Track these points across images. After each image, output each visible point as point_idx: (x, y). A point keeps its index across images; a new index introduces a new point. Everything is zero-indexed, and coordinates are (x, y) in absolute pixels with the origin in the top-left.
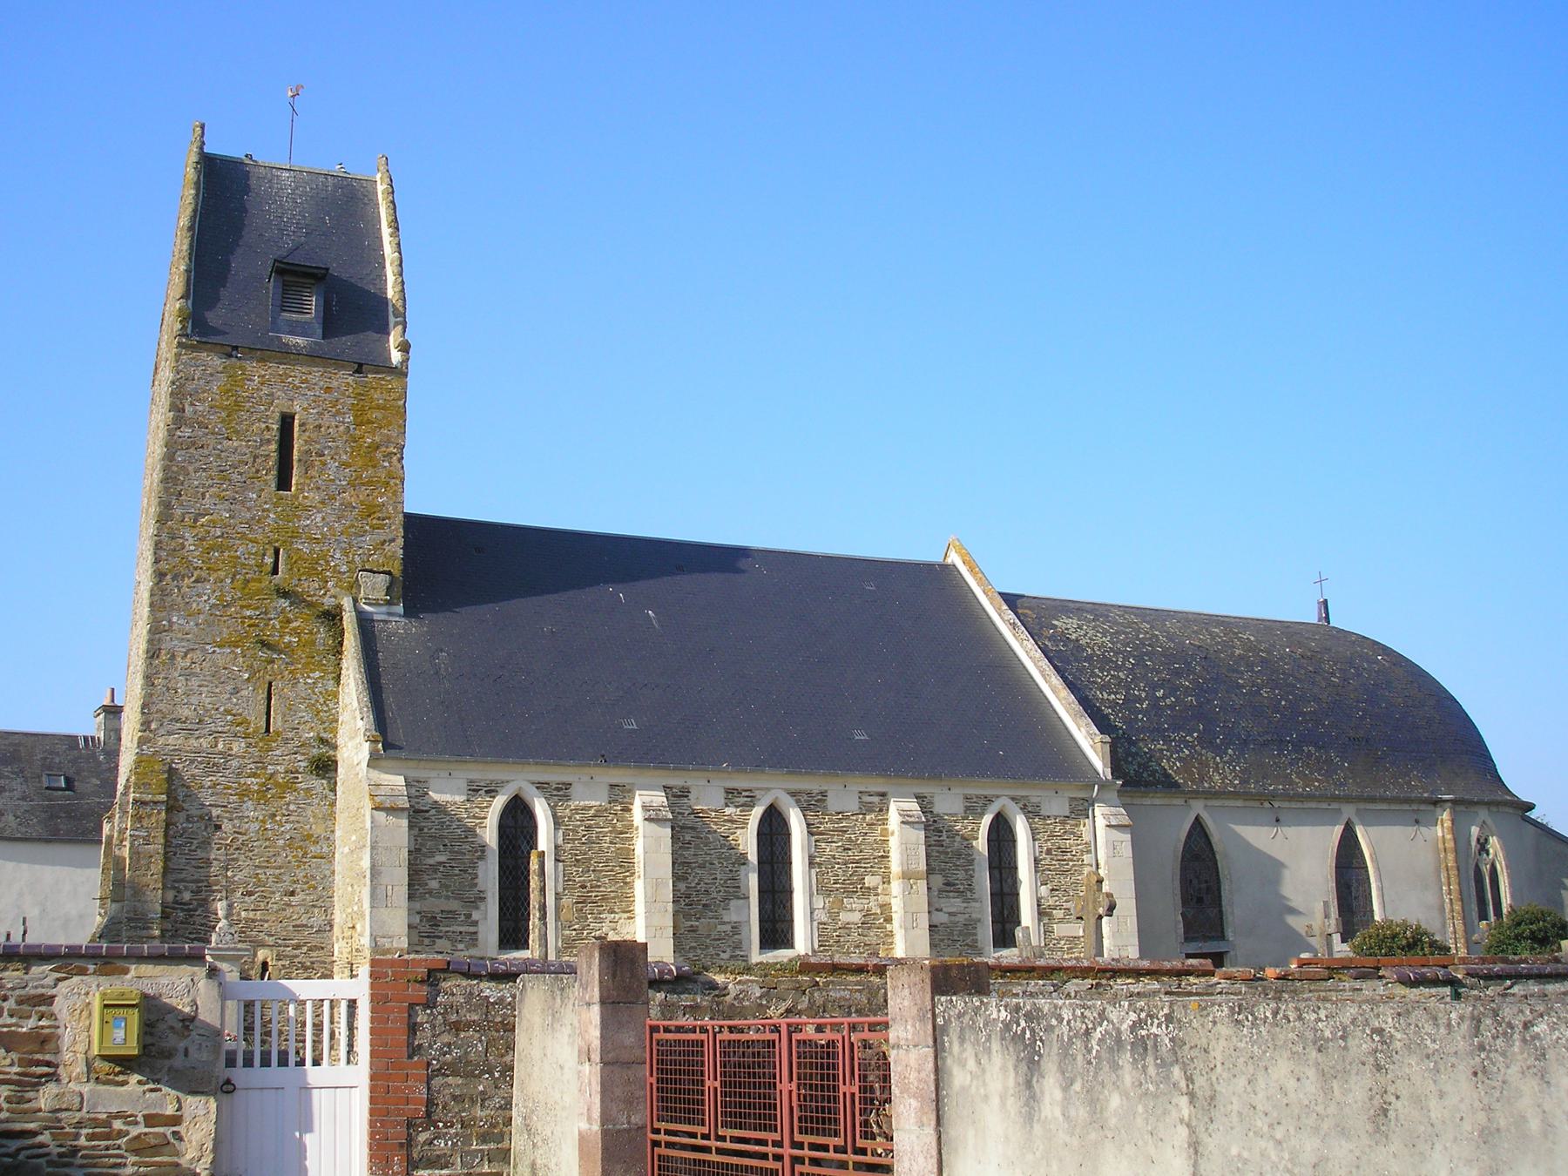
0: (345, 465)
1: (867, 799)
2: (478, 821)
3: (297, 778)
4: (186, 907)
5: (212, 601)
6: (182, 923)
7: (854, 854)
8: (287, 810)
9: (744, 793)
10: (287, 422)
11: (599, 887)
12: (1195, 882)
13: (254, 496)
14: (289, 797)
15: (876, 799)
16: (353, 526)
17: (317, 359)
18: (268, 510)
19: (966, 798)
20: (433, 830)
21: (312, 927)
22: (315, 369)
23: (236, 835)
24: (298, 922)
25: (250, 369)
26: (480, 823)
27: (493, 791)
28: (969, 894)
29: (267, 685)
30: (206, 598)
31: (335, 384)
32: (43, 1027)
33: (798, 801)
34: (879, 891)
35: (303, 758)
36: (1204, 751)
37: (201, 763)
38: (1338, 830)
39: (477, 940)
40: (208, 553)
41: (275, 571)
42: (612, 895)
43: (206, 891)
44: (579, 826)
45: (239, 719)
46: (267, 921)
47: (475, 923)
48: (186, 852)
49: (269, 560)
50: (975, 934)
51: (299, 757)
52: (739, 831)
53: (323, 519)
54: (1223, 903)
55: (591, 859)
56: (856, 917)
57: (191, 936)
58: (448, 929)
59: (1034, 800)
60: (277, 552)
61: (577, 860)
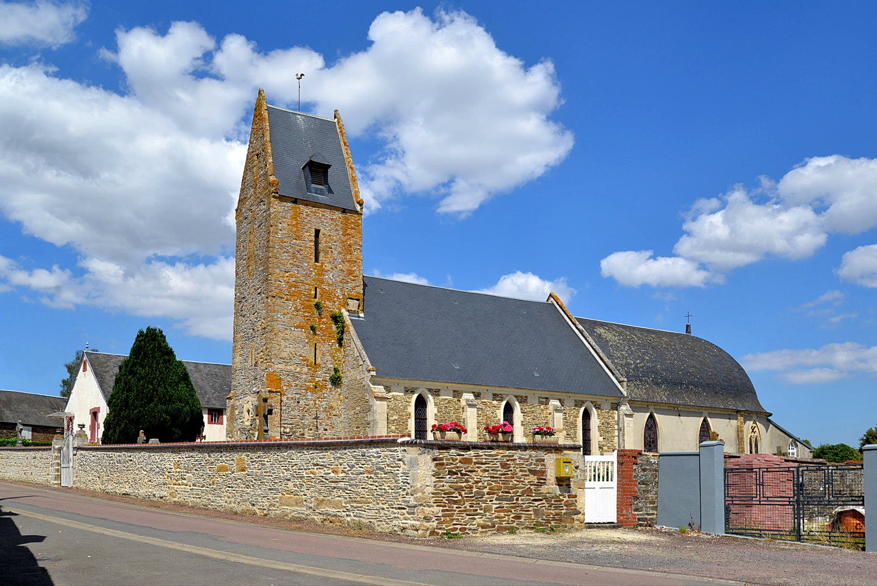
0: (340, 253)
1: (541, 400)
2: (408, 403)
4: (287, 434)
5: (293, 309)
8: (323, 396)
9: (499, 396)
10: (317, 232)
12: (648, 438)
13: (306, 265)
14: (324, 391)
15: (544, 400)
16: (344, 280)
18: (311, 271)
22: (327, 210)
27: (413, 392)
28: (575, 439)
29: (314, 345)
30: (290, 307)
31: (334, 217)
32: (542, 468)
33: (518, 400)
36: (654, 386)
37: (291, 376)
38: (702, 419)
41: (315, 297)
45: (305, 358)
48: (287, 412)
49: (313, 292)
51: (328, 375)
52: (497, 411)
53: (333, 276)
54: (658, 448)
55: (447, 420)
60: (316, 288)
61: (442, 420)
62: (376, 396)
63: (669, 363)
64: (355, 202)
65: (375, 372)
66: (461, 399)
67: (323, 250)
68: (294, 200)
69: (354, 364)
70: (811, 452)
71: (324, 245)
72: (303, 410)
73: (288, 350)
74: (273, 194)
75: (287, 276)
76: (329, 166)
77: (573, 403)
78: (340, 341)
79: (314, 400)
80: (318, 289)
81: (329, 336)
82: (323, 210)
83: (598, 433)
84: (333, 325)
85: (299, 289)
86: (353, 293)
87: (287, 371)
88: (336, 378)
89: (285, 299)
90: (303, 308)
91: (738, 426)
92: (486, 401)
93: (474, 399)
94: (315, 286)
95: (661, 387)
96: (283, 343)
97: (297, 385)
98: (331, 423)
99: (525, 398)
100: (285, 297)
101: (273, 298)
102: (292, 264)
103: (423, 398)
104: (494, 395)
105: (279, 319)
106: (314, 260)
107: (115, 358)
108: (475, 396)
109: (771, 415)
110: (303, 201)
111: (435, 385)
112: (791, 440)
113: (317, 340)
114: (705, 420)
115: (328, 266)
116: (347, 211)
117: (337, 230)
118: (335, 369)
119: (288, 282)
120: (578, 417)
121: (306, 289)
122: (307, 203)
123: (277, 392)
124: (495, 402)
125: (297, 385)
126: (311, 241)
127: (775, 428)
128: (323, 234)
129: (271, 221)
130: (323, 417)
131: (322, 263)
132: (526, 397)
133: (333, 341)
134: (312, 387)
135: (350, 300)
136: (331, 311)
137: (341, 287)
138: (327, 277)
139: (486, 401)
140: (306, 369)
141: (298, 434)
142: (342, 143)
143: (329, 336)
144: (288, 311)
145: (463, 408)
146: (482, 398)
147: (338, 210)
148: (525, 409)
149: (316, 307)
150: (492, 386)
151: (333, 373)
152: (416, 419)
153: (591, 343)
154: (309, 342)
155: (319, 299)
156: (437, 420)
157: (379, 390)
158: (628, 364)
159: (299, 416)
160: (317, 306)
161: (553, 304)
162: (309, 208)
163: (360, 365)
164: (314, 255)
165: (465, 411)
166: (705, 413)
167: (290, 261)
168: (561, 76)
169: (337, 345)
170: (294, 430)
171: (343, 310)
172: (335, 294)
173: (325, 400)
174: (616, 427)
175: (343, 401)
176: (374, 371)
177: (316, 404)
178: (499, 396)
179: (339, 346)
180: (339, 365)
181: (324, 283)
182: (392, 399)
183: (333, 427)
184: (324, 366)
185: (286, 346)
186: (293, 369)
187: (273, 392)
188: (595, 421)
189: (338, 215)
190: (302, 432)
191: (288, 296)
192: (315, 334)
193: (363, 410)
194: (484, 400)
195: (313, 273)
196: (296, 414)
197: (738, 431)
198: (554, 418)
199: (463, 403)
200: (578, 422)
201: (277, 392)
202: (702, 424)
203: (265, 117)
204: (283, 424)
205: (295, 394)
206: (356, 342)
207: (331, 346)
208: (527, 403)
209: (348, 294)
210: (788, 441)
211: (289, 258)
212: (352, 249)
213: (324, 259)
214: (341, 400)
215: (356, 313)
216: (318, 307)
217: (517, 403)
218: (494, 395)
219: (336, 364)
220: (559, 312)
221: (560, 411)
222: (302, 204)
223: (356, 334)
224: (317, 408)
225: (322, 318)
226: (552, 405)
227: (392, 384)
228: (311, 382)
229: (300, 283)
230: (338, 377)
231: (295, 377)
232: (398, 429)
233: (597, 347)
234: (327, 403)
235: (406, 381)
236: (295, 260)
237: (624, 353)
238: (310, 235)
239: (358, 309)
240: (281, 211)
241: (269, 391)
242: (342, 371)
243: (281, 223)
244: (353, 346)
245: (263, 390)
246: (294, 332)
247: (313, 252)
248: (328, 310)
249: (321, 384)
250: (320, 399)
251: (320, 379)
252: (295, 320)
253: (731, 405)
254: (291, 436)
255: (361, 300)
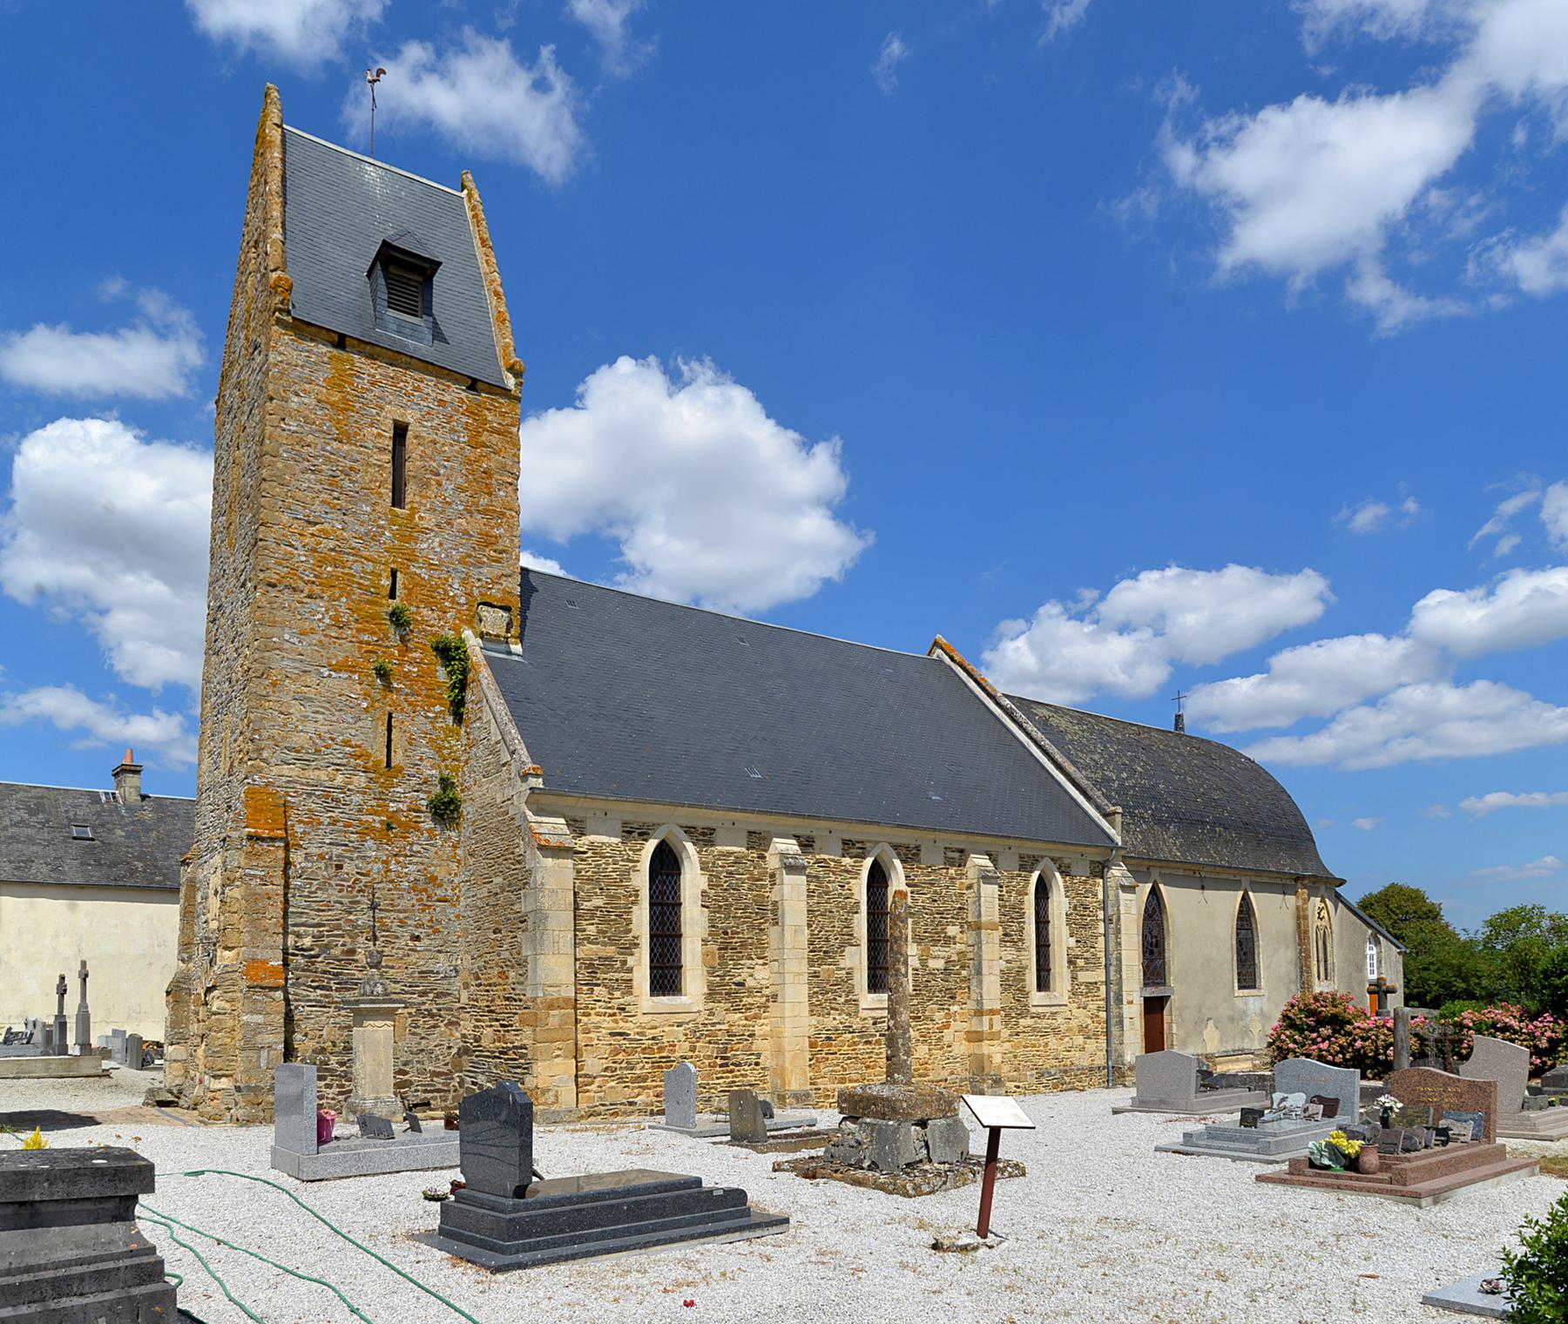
0: (462, 489)
1: (950, 855)
2: (631, 864)
3: (420, 817)
5: (327, 621)
6: (303, 970)
7: (940, 905)
8: (411, 850)
9: (857, 845)
10: (400, 431)
11: (738, 933)
13: (368, 509)
14: (412, 838)
15: (956, 855)
16: (470, 556)
17: (430, 367)
18: (382, 527)
19: (1021, 857)
20: (590, 873)
21: (438, 973)
23: (359, 876)
24: (424, 969)
25: (358, 364)
26: (634, 866)
28: (1020, 944)
29: (387, 717)
30: (320, 616)
31: (447, 398)
33: (899, 855)
34: (957, 940)
35: (424, 796)
36: (1156, 827)
39: (631, 987)
40: (321, 567)
41: (392, 595)
42: (750, 941)
43: (328, 936)
44: (722, 872)
46: (393, 967)
47: (630, 970)
48: (306, 894)
49: (386, 582)
50: (1024, 980)
51: (422, 795)
52: (852, 881)
54: (1166, 955)
55: (731, 905)
56: (940, 964)
57: (313, 984)
58: (605, 976)
59: (1066, 861)
60: (394, 574)
61: (720, 907)
62: (543, 843)
63: (1179, 780)
64: (503, 369)
65: (540, 780)
66: (766, 854)
67: (414, 477)
68: (336, 338)
69: (489, 764)
70: (1399, 953)
71: (418, 463)
72: (354, 888)
73: (310, 727)
74: (277, 314)
75: (313, 535)
76: (440, 264)
77: (1017, 862)
78: (457, 708)
79: (384, 862)
80: (399, 574)
81: (427, 696)
82: (417, 375)
83: (1065, 930)
84: (438, 668)
85: (346, 571)
86: (495, 593)
87: (308, 784)
88: (444, 803)
89: (306, 592)
90: (356, 621)
91: (1298, 908)
92: (826, 857)
93: (800, 852)
94: (392, 566)
95: (1169, 829)
96: (295, 708)
97: (334, 822)
98: (431, 920)
99: (915, 851)
100: (307, 589)
101: (270, 589)
102: (328, 504)
103: (671, 851)
104: (845, 842)
105: (287, 645)
106: (389, 500)
107: (24, 791)
108: (801, 845)
109: (1342, 882)
110: (363, 346)
111: (703, 818)
112: (1370, 931)
113: (395, 704)
114: (1245, 899)
115: (428, 520)
116: (480, 385)
117: (453, 431)
118: (442, 780)
119: (315, 550)
120: (1027, 894)
121: (364, 572)
122: (373, 351)
123: (273, 839)
124: (847, 861)
125: (334, 822)
126: (381, 450)
127: (1346, 910)
128: (416, 437)
129: (271, 387)
130: (409, 904)
131: (412, 508)
132: (918, 848)
133: (438, 708)
134: (377, 825)
135: (485, 608)
136: (434, 635)
137: (463, 576)
138: (425, 546)
139: (826, 857)
140: (363, 779)
141: (336, 952)
142: (477, 242)
143: (427, 696)
144: (315, 625)
145: (773, 876)
146: (817, 850)
147: (456, 382)
148: (915, 875)
149: (392, 622)
150: (842, 820)
151: (438, 790)
152: (651, 905)
153: (1033, 734)
154: (371, 710)
155: (402, 600)
156: (707, 907)
157: (553, 827)
158: (1108, 780)
159: (341, 903)
160: (397, 618)
161: (941, 661)
162: (379, 366)
163: (504, 765)
164: (390, 487)
165: (777, 882)
166: (1246, 882)
167: (324, 496)
168: (848, 461)
169: (450, 719)
170: (326, 940)
171: (468, 633)
172: (445, 590)
173: (415, 860)
174: (1101, 914)
175: (463, 863)
176: (537, 776)
177: (390, 871)
178: (857, 845)
179: (454, 722)
180: (456, 769)
181: (417, 562)
182: (590, 854)
183: (437, 931)
184: (413, 771)
185: (306, 717)
186: (324, 777)
187: (263, 840)
188: (1059, 903)
189: (456, 393)
190: (349, 946)
191: (314, 587)
192: (388, 688)
193: (510, 885)
194: (823, 856)
195: (387, 534)
196: (333, 898)
197: (1298, 918)
198: (979, 897)
199: (773, 862)
200: (1026, 906)
201: (273, 839)
202: (1241, 905)
203: (273, 139)
204: (294, 925)
205: (330, 844)
206: (493, 705)
207: (434, 721)
208: (919, 862)
209: (481, 594)
210: (1365, 934)
211: (319, 487)
212: (494, 481)
213: (418, 499)
214: (459, 862)
215: (499, 642)
216: (398, 620)
217: (897, 862)
218: (845, 842)
219: (447, 766)
220: (957, 674)
221: (993, 881)
222: (359, 353)
223: (494, 686)
224: (392, 881)
225: (408, 650)
226: (975, 866)
227: (590, 814)
228: (376, 813)
229: (349, 554)
230: (451, 801)
231: (330, 798)
232: (604, 932)
233: (1046, 743)
234: (421, 867)
235: (628, 806)
236: (336, 494)
237: (1096, 757)
238: (380, 435)
239: (508, 631)
240: (300, 363)
241: (250, 837)
242: (462, 785)
243: (298, 395)
244: (487, 716)
245: (234, 834)
246: (329, 680)
247: (386, 480)
248: (424, 630)
249: (403, 819)
250: (401, 859)
251: (401, 806)
252: (332, 650)
253: (1286, 866)
254: (317, 956)
255: (515, 611)
